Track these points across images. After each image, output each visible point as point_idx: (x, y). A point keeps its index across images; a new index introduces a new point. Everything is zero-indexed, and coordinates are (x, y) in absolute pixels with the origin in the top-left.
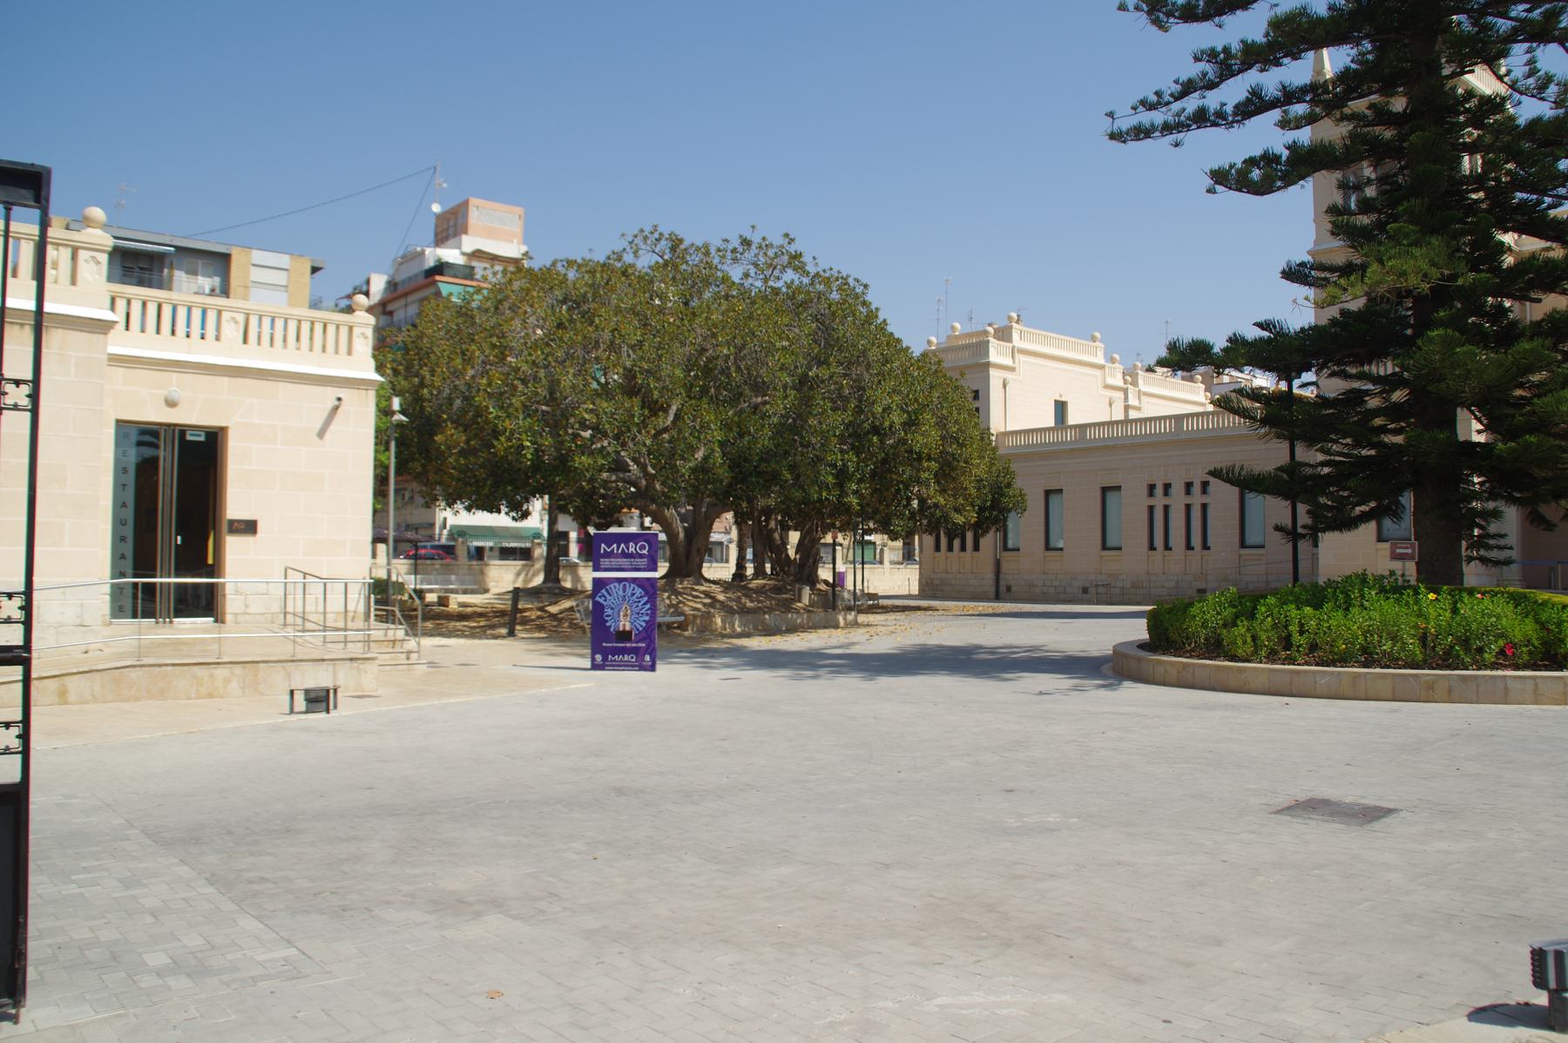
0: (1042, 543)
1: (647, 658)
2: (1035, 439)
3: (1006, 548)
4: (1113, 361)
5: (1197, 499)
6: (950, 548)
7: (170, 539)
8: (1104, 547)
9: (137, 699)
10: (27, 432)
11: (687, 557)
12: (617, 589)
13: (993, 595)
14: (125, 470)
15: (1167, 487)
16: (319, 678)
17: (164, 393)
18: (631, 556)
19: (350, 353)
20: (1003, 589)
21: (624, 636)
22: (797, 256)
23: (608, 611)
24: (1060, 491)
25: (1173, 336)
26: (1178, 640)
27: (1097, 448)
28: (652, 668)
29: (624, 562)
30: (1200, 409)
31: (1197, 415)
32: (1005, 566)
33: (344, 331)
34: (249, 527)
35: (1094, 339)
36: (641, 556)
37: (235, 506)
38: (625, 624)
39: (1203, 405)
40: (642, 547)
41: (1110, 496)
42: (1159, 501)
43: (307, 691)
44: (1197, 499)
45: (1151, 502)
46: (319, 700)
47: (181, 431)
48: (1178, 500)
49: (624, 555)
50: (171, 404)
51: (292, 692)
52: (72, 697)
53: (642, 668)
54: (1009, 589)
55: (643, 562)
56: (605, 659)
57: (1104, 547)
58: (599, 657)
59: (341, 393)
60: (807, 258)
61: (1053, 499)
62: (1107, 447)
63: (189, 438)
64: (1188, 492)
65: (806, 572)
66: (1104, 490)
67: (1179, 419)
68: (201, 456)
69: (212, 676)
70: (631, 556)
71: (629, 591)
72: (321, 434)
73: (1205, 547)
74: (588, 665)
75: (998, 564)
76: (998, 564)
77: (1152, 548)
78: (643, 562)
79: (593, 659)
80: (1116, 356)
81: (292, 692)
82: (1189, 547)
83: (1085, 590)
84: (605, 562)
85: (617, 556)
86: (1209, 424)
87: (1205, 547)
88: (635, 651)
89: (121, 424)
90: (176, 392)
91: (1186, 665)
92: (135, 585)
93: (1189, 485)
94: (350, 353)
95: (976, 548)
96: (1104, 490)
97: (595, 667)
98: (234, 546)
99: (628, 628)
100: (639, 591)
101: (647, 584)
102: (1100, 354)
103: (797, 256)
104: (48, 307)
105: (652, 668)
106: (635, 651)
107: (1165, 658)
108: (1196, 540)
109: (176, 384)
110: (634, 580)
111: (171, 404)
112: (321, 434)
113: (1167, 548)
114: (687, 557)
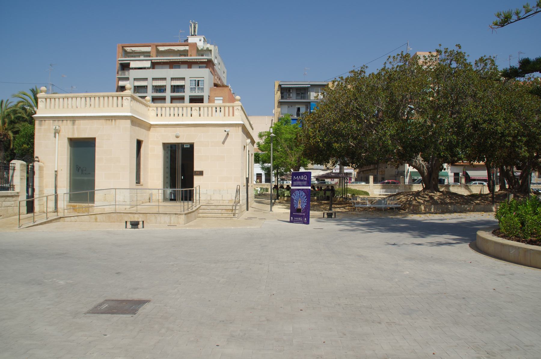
7: (180, 177)
9: (114, 222)
14: (167, 158)
16: (136, 218)
17: (175, 134)
19: (233, 115)
23: (295, 201)
25: (525, 56)
29: (300, 183)
33: (231, 109)
34: (201, 173)
36: (305, 180)
37: (196, 168)
38: (299, 206)
40: (305, 177)
43: (131, 222)
46: (135, 225)
47: (183, 144)
50: (177, 137)
51: (126, 222)
52: (98, 221)
53: (304, 223)
55: (305, 183)
56: (293, 219)
59: (227, 129)
68: (187, 152)
69: (134, 217)
71: (301, 194)
72: (223, 143)
74: (289, 220)
78: (305, 183)
81: (126, 222)
89: (164, 145)
90: (179, 134)
92: (182, 191)
94: (233, 115)
98: (196, 179)
100: (304, 194)
101: (306, 191)
109: (179, 131)
110: (303, 189)
111: (177, 137)
112: (223, 143)
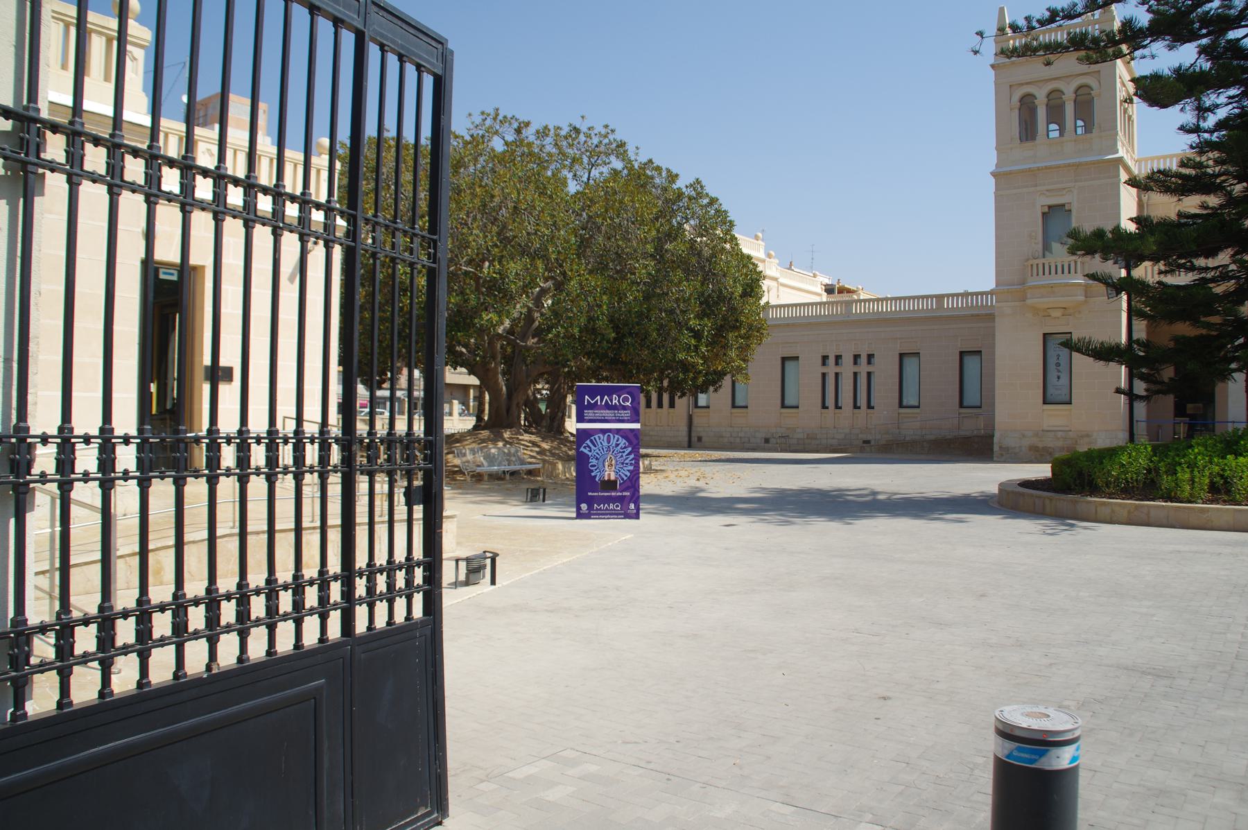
0: (779, 402)
1: (632, 506)
2: (885, 307)
3: (696, 406)
4: (769, 256)
5: (863, 368)
6: (660, 405)
8: (734, 406)
10: (63, 253)
11: (508, 411)
12: (602, 440)
13: (686, 444)
15: (838, 358)
18: (614, 408)
20: (694, 439)
21: (610, 485)
22: (622, 145)
23: (594, 462)
24: (797, 358)
26: (1075, 485)
27: (779, 325)
28: (637, 516)
29: (608, 413)
30: (817, 299)
31: (816, 304)
32: (696, 421)
35: (757, 238)
36: (624, 408)
39: (820, 295)
40: (626, 400)
41: (789, 365)
42: (831, 369)
44: (863, 368)
45: (825, 370)
48: (847, 369)
49: (608, 407)
53: (627, 516)
54: (700, 439)
55: (626, 414)
56: (590, 507)
57: (783, 406)
58: (584, 506)
60: (630, 148)
61: (790, 365)
62: (788, 325)
63: (162, 276)
64: (824, 364)
65: (555, 424)
66: (784, 359)
67: (940, 298)
70: (614, 408)
71: (613, 442)
73: (870, 407)
74: (574, 515)
75: (690, 418)
76: (690, 418)
77: (824, 407)
78: (626, 414)
79: (579, 509)
80: (772, 253)
82: (856, 407)
83: (767, 441)
84: (589, 414)
85: (601, 408)
86: (824, 311)
87: (870, 407)
88: (621, 500)
91: (1137, 507)
93: (856, 358)
95: (672, 405)
96: (784, 359)
97: (580, 516)
99: (613, 478)
100: (623, 442)
101: (631, 436)
102: (762, 251)
103: (622, 145)
104: (87, 105)
105: (637, 516)
106: (621, 500)
107: (1089, 499)
108: (862, 401)
110: (618, 431)
113: (837, 407)
114: (508, 411)
